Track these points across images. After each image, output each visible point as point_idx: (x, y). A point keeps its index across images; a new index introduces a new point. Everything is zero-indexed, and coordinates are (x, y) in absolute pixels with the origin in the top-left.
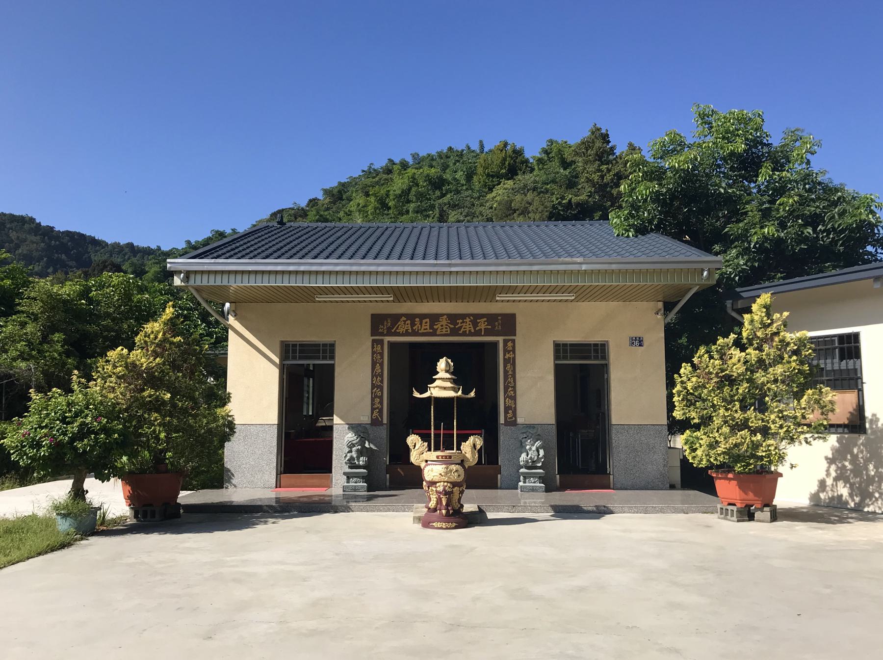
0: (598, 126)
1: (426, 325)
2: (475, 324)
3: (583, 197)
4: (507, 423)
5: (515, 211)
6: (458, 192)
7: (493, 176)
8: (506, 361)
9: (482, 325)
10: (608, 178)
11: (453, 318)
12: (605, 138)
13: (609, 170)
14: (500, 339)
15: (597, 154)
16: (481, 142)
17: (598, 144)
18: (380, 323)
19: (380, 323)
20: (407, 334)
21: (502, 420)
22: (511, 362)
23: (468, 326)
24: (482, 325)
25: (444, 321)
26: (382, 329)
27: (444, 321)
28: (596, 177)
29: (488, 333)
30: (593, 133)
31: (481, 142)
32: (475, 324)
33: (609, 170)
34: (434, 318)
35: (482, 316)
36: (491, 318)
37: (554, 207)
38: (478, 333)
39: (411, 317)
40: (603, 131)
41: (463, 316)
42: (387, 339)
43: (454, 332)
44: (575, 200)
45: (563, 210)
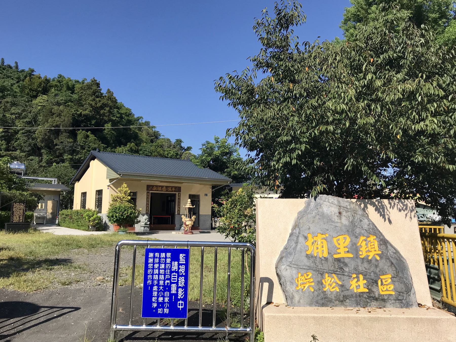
0: (96, 79)
1: (160, 189)
2: (172, 189)
3: (87, 112)
4: (178, 214)
5: (54, 114)
6: (15, 97)
7: (33, 91)
8: (178, 199)
9: (173, 189)
10: (99, 105)
11: (167, 187)
12: (98, 85)
13: (100, 101)
14: (177, 193)
15: (93, 92)
16: (3, 59)
17: (94, 87)
18: (149, 187)
19: (149, 187)
20: (155, 191)
21: (176, 213)
22: (179, 199)
23: (170, 189)
24: (173, 189)
25: (164, 188)
26: (150, 189)
27: (164, 188)
28: (93, 103)
29: (175, 191)
30: (93, 81)
31: (3, 59)
32: (172, 189)
33: (100, 101)
34: (162, 187)
35: (173, 187)
36: (176, 187)
37: (73, 115)
38: (172, 191)
39: (157, 186)
40: (98, 82)
41: (169, 187)
42: (151, 192)
43: (167, 191)
44: (84, 113)
45: (77, 117)
